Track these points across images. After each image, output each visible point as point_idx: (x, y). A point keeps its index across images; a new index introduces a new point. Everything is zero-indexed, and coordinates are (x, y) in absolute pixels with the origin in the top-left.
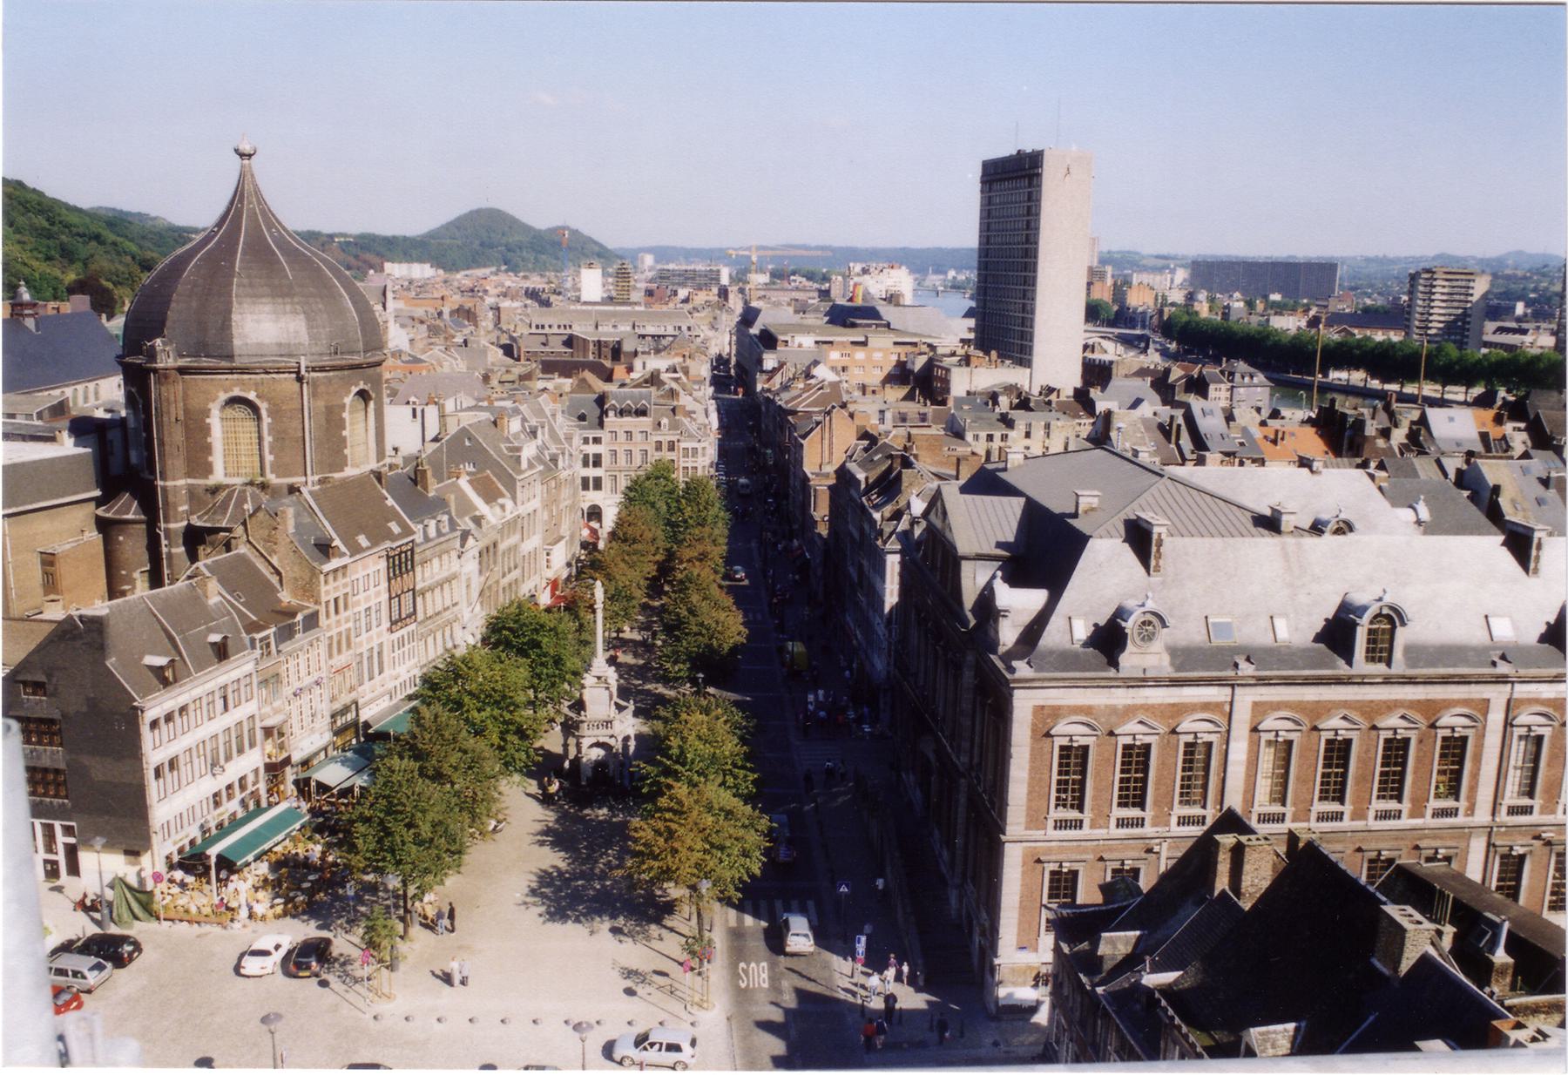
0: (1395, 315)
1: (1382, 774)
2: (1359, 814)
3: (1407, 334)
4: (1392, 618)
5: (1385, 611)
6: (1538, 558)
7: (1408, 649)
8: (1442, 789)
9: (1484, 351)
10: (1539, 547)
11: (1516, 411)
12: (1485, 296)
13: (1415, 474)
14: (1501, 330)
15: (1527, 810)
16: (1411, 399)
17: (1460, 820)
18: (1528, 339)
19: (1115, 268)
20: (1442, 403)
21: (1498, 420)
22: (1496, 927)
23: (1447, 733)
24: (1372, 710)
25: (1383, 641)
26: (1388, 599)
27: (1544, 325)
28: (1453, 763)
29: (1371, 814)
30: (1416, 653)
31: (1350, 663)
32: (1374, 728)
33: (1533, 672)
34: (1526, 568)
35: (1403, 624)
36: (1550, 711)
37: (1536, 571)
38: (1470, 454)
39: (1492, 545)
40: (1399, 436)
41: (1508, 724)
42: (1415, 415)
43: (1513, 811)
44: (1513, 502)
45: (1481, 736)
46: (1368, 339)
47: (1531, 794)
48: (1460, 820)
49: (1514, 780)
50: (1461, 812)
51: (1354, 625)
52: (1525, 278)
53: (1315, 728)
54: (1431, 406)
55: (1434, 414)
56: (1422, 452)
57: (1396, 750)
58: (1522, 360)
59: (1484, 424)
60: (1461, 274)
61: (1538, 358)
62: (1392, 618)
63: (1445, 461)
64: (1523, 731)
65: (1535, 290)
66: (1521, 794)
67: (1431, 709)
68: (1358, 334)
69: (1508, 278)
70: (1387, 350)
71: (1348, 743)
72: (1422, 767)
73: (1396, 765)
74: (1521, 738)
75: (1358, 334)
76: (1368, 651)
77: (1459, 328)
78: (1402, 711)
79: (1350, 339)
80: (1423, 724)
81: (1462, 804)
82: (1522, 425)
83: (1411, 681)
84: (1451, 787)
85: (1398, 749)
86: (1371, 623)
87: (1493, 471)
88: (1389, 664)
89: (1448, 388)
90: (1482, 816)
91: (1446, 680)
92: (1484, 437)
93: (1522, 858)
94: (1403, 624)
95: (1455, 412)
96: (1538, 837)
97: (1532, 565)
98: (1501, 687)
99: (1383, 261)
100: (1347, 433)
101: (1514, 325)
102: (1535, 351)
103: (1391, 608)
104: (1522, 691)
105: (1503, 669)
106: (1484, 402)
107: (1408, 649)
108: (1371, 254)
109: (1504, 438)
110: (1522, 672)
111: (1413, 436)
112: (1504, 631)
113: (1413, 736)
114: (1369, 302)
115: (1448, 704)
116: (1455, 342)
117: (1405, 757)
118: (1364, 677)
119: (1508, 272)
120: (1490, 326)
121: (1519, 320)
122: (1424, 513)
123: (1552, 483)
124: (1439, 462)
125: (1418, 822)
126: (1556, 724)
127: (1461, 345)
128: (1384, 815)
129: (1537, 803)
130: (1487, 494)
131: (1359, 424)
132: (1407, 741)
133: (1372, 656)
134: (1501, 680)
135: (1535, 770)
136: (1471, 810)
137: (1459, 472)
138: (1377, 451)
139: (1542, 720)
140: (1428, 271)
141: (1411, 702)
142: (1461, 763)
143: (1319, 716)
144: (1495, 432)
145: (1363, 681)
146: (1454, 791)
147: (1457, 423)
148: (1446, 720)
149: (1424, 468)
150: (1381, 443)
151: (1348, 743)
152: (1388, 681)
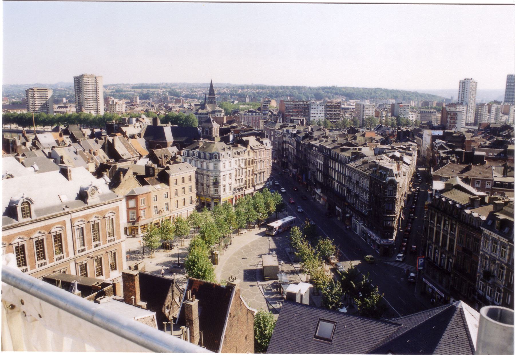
0: (24, 104)
1: (37, 252)
2: (33, 267)
3: (28, 110)
4: (28, 203)
5: (25, 200)
6: (70, 175)
7: (36, 211)
8: (57, 251)
9: (55, 114)
10: (70, 172)
11: (66, 132)
12: (52, 96)
13: (36, 156)
14: (59, 107)
15: (84, 250)
16: (32, 132)
17: (65, 259)
18: (68, 109)
19: (105, 87)
20: (43, 132)
21: (61, 135)
22: (74, 284)
23: (55, 234)
24: (28, 233)
25: (27, 210)
26: (25, 197)
27: (72, 105)
28: (59, 243)
29: (37, 266)
30: (38, 212)
31: (17, 220)
32: (31, 238)
33: (76, 209)
34: (68, 179)
35: (32, 203)
36: (83, 219)
37: (71, 179)
38: (53, 147)
39: (56, 174)
40: (29, 144)
41: (72, 226)
42: (33, 137)
43: (80, 251)
44: (68, 160)
45: (65, 232)
46: (15, 113)
47: (84, 245)
48: (65, 259)
49: (78, 242)
50: (65, 257)
51: (15, 208)
52: (65, 90)
53: (10, 244)
54: (38, 133)
55: (39, 136)
56: (38, 149)
57: (40, 244)
58: (67, 116)
59: (56, 138)
60: (43, 90)
61: (71, 115)
62: (28, 203)
63: (45, 150)
64: (77, 227)
65: (68, 94)
66: (81, 246)
67: (48, 228)
68: (12, 112)
69: (59, 90)
70: (22, 117)
71: (23, 246)
72: (49, 246)
73: (41, 248)
74: (77, 229)
75: (12, 112)
76: (22, 214)
77: (45, 107)
78: (38, 231)
79: (8, 114)
80: (46, 233)
81: (65, 254)
82: (68, 136)
83: (39, 221)
84: (60, 250)
85: (40, 243)
86: (22, 205)
87: (60, 151)
88: (31, 217)
89: (46, 127)
90: (72, 256)
91: (50, 218)
92: (57, 141)
93: (86, 264)
94: (32, 203)
95: (46, 134)
96: (89, 257)
97: (69, 177)
98: (67, 216)
99: (16, 86)
100: (11, 146)
101: (63, 105)
102: (70, 113)
103: (27, 199)
104: (74, 215)
105: (67, 210)
106: (56, 130)
107: (36, 211)
108: (12, 84)
109: (63, 141)
110: (73, 210)
111: (34, 144)
112: (65, 199)
113: (44, 238)
114: (14, 100)
115: (53, 225)
116: (45, 112)
117: (43, 245)
118: (23, 223)
119: (59, 88)
120: (56, 106)
121: (64, 104)
122: (37, 168)
123: (78, 153)
124: (43, 151)
125: (52, 264)
126: (86, 223)
127: (47, 113)
128: (42, 265)
129: (86, 247)
130: (59, 159)
131: (14, 142)
132: (42, 240)
133: (24, 215)
134: (67, 214)
135: (83, 238)
136: (68, 255)
137: (49, 153)
138: (22, 150)
139: (82, 223)
140: (32, 89)
141: (41, 227)
142: (61, 242)
143: (10, 240)
144: (60, 139)
145: (23, 225)
146: (61, 251)
147: (48, 138)
148: (53, 230)
149: (38, 153)
150: (23, 147)
151: (23, 246)
152: (31, 223)
